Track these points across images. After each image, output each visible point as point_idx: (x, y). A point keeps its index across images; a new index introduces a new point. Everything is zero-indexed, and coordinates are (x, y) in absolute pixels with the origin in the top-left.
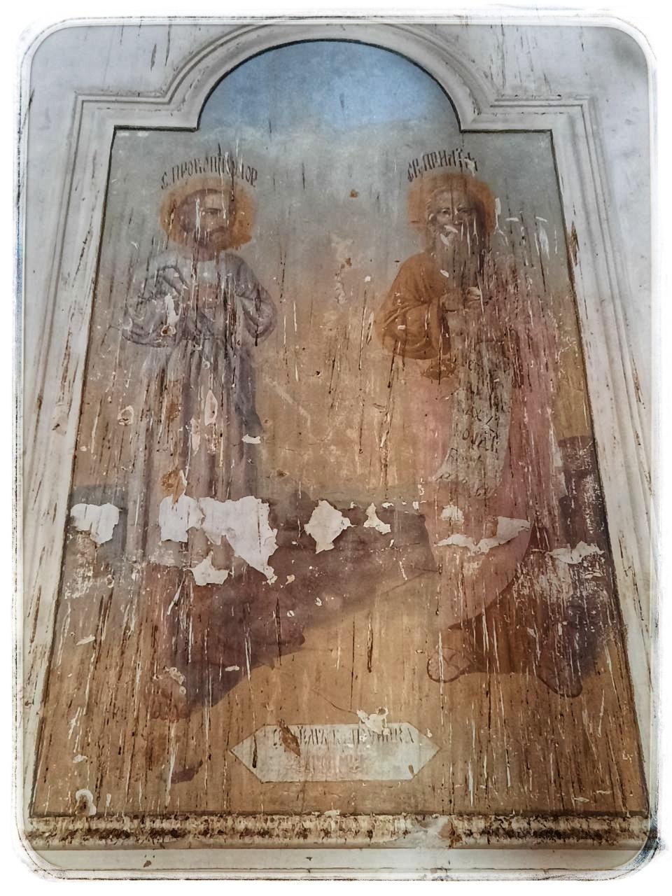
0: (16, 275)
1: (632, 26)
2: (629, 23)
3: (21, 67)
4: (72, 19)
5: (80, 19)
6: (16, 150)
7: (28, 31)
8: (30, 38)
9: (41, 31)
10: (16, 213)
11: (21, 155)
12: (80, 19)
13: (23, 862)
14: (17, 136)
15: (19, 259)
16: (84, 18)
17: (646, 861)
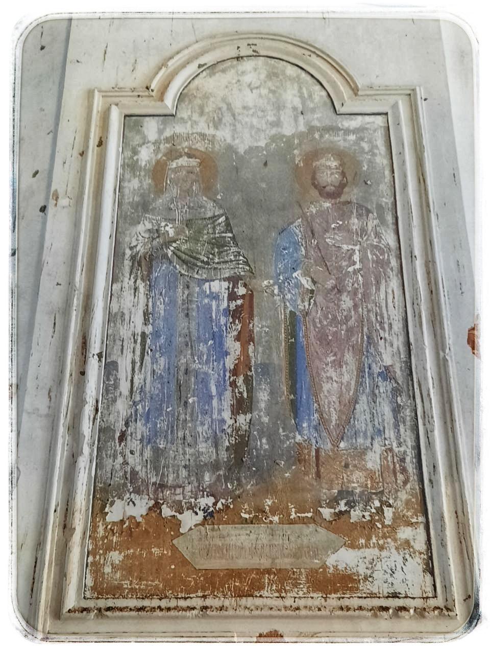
2: (458, 17)
3: (16, 48)
4: (52, 14)
5: (58, 14)
6: (12, 110)
7: (20, 23)
8: (22, 28)
9: (30, 23)
10: (12, 156)
11: (16, 113)
12: (58, 14)
13: (17, 629)
14: (12, 99)
16: (61, 13)
17: (471, 628)
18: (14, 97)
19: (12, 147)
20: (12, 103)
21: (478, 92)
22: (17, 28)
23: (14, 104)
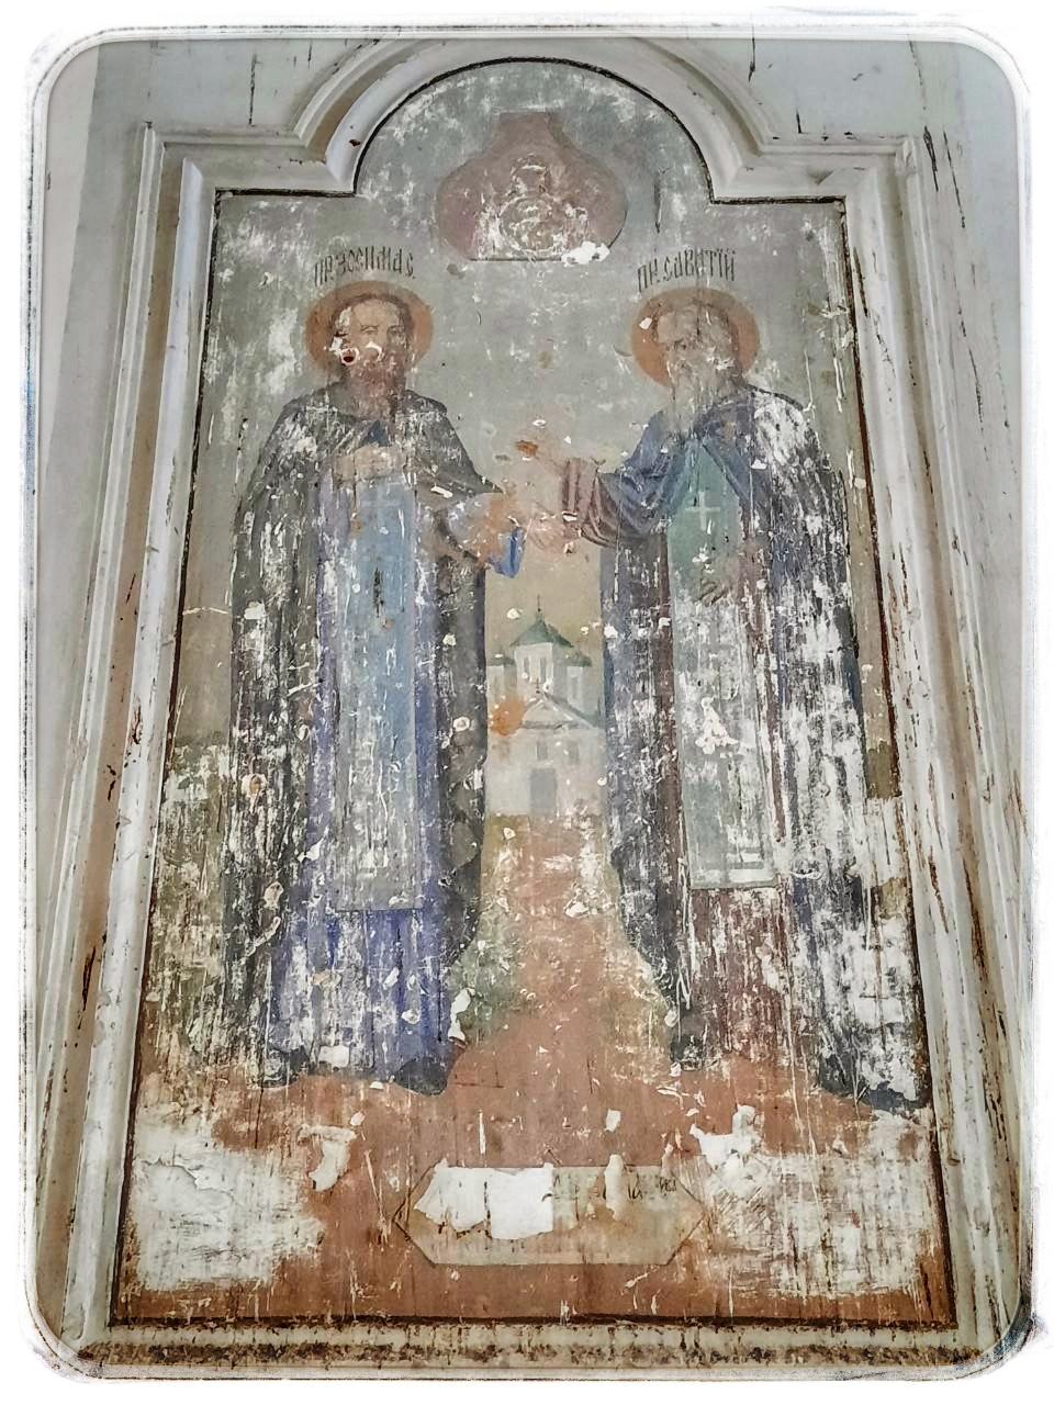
0: (25, 432)
1: (991, 40)
3: (34, 104)
6: (25, 235)
7: (44, 49)
8: (47, 60)
10: (25, 335)
11: (34, 244)
13: (37, 1351)
14: (26, 212)
15: (29, 407)
16: (132, 29)
18: (30, 207)
19: (25, 316)
20: (26, 222)
21: (1028, 198)
22: (36, 61)
23: (30, 223)
